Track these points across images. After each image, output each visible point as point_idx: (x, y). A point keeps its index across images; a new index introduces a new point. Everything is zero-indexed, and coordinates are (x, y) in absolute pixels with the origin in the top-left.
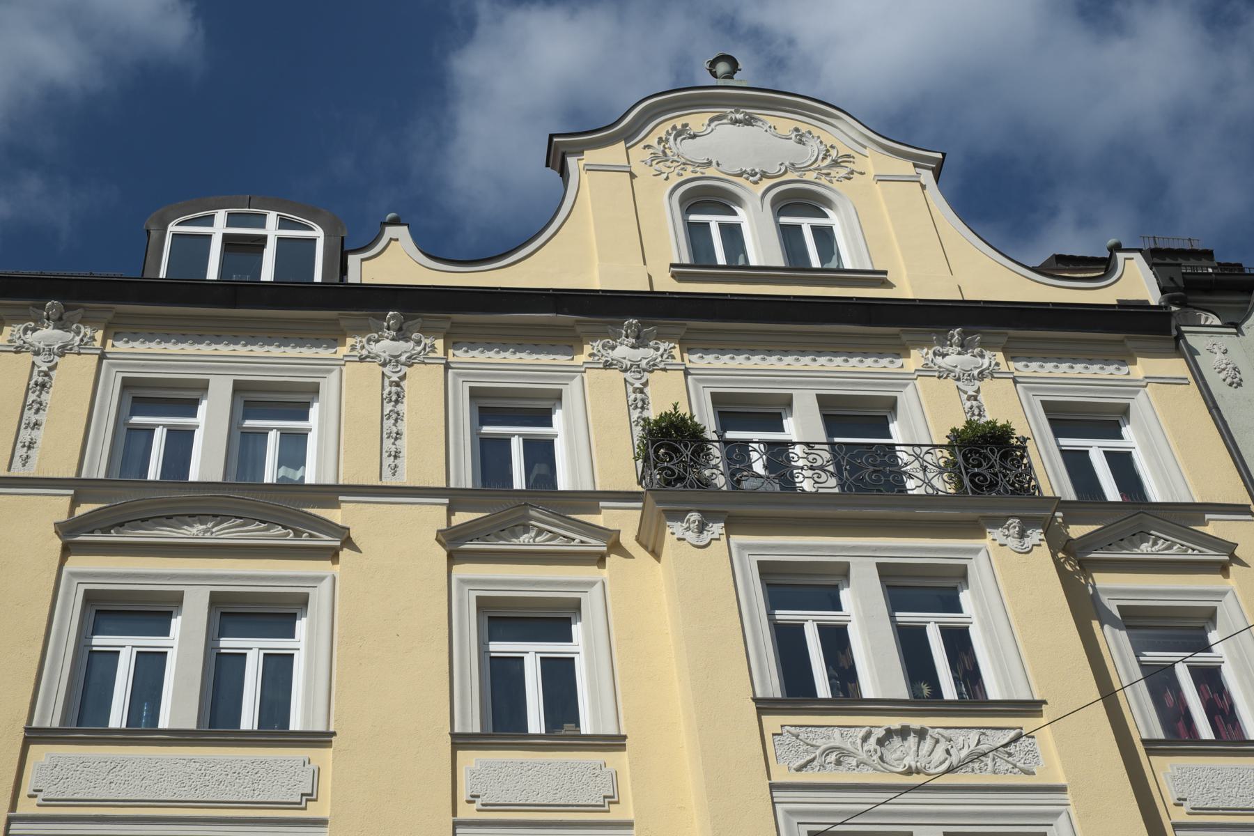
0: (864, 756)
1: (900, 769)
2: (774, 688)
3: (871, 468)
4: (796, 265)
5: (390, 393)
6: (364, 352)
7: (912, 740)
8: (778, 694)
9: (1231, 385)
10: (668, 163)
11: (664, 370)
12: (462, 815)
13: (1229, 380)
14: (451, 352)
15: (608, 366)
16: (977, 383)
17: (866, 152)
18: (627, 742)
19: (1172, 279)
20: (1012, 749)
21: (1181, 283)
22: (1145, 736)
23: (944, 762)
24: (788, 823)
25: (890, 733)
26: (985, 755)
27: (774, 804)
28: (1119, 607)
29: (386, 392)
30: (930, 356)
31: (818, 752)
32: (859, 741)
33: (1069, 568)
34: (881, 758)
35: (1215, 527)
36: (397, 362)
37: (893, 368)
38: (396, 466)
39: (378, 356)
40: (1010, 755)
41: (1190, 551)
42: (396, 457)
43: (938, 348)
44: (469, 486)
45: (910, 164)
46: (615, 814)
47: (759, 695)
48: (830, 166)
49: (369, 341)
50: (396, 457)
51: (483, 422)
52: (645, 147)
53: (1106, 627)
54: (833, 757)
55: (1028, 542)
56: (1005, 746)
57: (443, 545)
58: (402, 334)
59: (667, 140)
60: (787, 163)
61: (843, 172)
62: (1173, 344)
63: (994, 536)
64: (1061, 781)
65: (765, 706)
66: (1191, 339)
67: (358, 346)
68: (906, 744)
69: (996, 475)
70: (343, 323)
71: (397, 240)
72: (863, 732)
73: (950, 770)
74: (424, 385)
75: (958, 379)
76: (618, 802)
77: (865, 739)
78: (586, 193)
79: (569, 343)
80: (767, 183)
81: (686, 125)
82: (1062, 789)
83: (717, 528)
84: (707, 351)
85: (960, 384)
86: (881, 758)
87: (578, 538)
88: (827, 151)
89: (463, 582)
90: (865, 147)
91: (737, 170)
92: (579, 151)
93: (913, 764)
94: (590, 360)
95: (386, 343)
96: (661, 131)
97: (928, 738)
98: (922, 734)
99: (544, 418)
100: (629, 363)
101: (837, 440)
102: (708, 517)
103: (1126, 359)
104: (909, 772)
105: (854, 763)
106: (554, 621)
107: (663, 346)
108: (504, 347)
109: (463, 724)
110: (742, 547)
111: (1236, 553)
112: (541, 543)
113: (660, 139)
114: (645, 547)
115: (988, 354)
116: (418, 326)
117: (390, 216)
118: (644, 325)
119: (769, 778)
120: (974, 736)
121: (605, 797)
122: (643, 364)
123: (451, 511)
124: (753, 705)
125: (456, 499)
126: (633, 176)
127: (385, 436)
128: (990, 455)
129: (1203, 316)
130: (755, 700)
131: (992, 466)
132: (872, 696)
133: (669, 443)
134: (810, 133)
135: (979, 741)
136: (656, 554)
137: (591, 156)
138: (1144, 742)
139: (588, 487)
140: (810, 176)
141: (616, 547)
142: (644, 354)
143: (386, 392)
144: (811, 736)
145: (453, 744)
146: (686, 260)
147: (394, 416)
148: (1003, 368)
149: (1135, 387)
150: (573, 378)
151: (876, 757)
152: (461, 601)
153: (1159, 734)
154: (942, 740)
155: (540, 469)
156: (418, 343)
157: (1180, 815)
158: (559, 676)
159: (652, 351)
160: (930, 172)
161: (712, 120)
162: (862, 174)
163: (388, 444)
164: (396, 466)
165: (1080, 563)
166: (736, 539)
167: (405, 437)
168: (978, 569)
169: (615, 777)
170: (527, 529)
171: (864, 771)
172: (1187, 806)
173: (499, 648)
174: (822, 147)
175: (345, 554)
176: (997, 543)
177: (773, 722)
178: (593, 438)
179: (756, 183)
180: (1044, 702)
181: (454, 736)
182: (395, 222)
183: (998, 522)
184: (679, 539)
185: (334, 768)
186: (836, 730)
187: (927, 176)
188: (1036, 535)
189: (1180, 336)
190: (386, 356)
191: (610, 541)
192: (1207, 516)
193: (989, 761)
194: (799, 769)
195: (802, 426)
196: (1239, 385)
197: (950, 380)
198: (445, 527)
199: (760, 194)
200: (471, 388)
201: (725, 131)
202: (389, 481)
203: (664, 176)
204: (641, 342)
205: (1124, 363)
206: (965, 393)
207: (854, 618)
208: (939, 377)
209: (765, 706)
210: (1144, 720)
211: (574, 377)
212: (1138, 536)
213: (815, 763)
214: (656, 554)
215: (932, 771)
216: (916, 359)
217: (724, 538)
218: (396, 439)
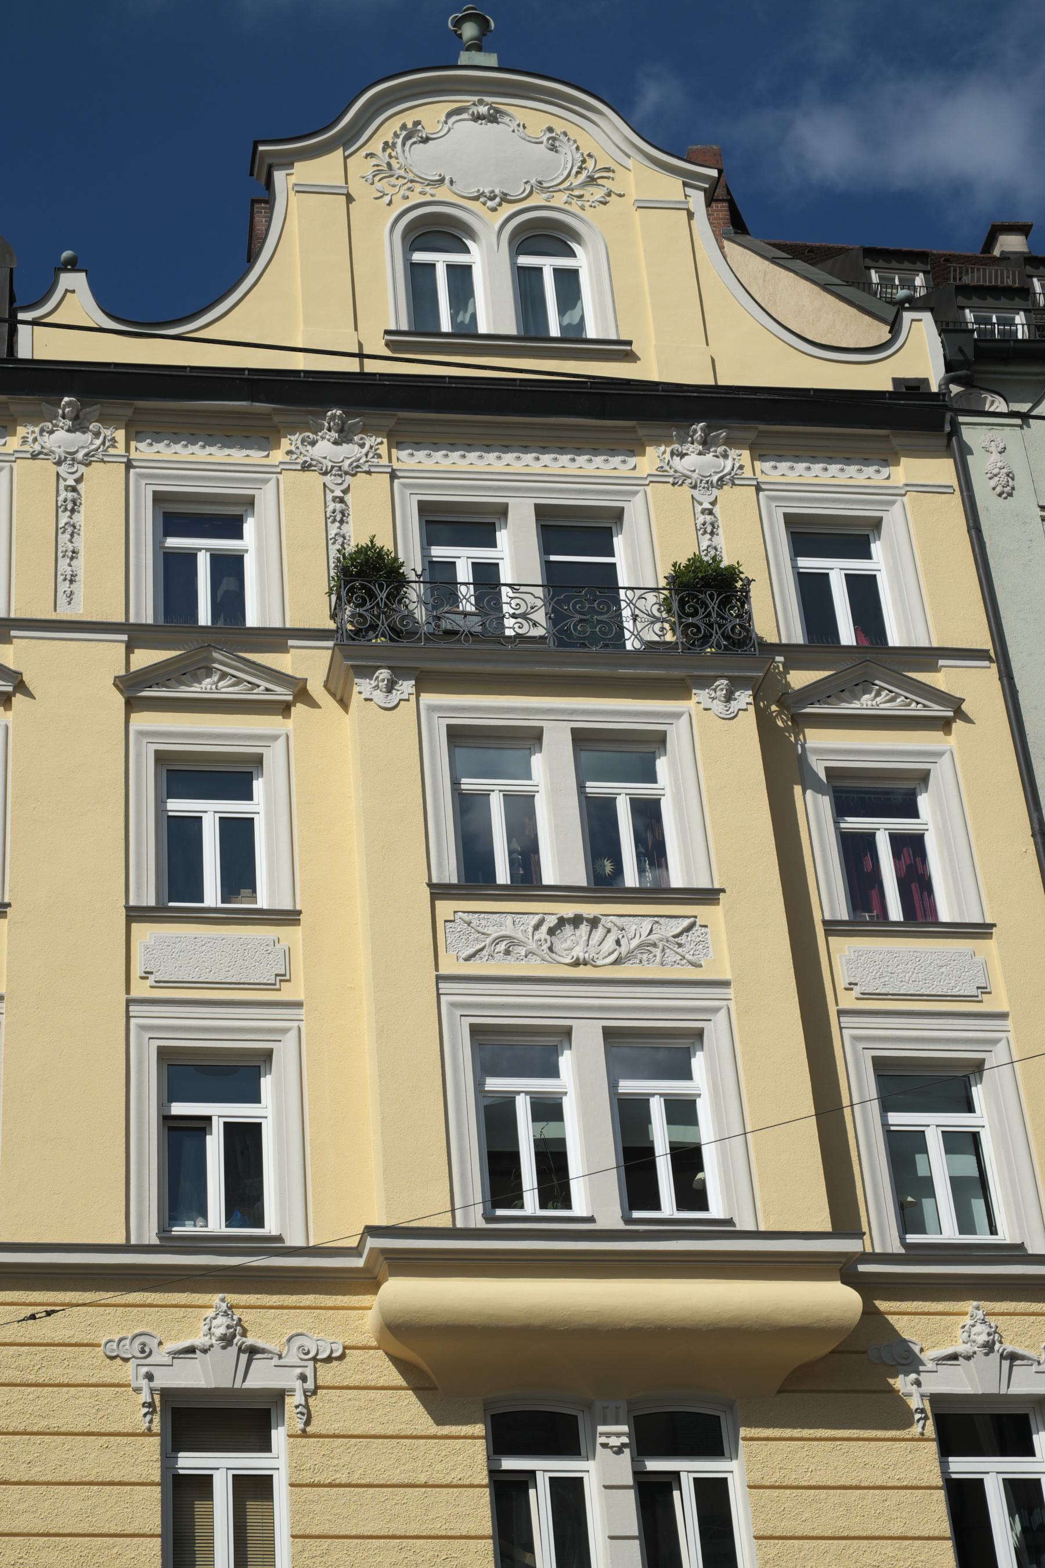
0: (533, 946)
1: (568, 960)
2: (449, 872)
3: (578, 617)
4: (531, 335)
5: (65, 501)
6: (37, 447)
7: (584, 928)
8: (454, 880)
9: (1000, 495)
10: (393, 180)
11: (369, 473)
12: (135, 994)
13: (999, 489)
14: (133, 444)
15: (306, 467)
16: (715, 492)
17: (629, 163)
18: (302, 917)
19: (961, 350)
20: (682, 940)
21: (971, 355)
22: (827, 917)
23: (613, 953)
24: (451, 1015)
25: (562, 922)
26: (655, 945)
27: (439, 995)
28: (827, 769)
29: (61, 499)
30: (667, 456)
31: (488, 941)
32: (530, 929)
33: (780, 723)
34: (551, 949)
35: (943, 678)
36: (73, 459)
37: (624, 470)
38: (72, 593)
39: (53, 452)
40: (680, 945)
41: (914, 704)
42: (71, 581)
43: (676, 446)
44: (150, 621)
45: (678, 182)
46: (286, 994)
47: (435, 881)
48: (584, 185)
49: (42, 431)
50: (71, 581)
51: (168, 533)
52: (367, 156)
53: (809, 792)
54: (502, 947)
55: (734, 706)
56: (675, 936)
57: (121, 691)
58: (78, 425)
59: (394, 144)
60: (533, 181)
61: (598, 193)
62: (945, 442)
63: (701, 696)
64: (727, 976)
65: (439, 891)
66: (969, 435)
67: (30, 440)
68: (578, 932)
69: (711, 626)
70: (13, 408)
71: (73, 292)
72: (534, 920)
73: (617, 962)
74: (102, 485)
75: (695, 487)
76: (289, 981)
77: (537, 927)
78: (294, 224)
79: (265, 436)
80: (508, 210)
81: (417, 123)
82: (726, 984)
83: (407, 687)
84: (418, 445)
85: (695, 493)
86: (551, 949)
87: (264, 684)
88: (584, 161)
89: (141, 734)
90: (629, 156)
91: (473, 191)
92: (288, 161)
93: (581, 956)
94: (287, 459)
95: (61, 435)
96: (387, 134)
97: (600, 926)
98: (594, 922)
99: (233, 527)
100: (330, 464)
101: (553, 558)
102: (399, 673)
103: (889, 459)
104: (576, 963)
105: (523, 953)
106: (233, 777)
107: (370, 441)
108: (192, 439)
109: (138, 896)
110: (432, 709)
111: (964, 707)
112: (226, 690)
113: (386, 143)
114: (333, 695)
115: (733, 453)
116: (97, 413)
117: (67, 254)
118: (349, 415)
119: (437, 969)
120: (647, 924)
121: (277, 975)
122: (346, 465)
123: (130, 649)
124: (426, 892)
125: (136, 636)
126: (350, 199)
127: (60, 555)
128: (708, 600)
129: (990, 399)
130: (430, 885)
131: (709, 615)
132: (552, 883)
133: (366, 577)
134: (565, 134)
135: (651, 931)
136: (344, 703)
137: (304, 171)
138: (825, 923)
139: (277, 624)
140: (559, 200)
141: (302, 694)
142: (350, 451)
143: (61, 499)
144: (484, 923)
145: (127, 916)
146: (404, 326)
147: (70, 530)
148: (748, 473)
149: (891, 495)
150: (266, 481)
151: (545, 947)
152: (138, 756)
153: (843, 913)
154: (614, 930)
155: (228, 584)
156: (97, 435)
157: (848, 1001)
158: (238, 836)
159: (356, 447)
160: (702, 194)
161: (449, 115)
162: (620, 196)
163: (63, 563)
164: (72, 593)
165: (794, 718)
166: (428, 699)
167: (82, 555)
168: (678, 735)
169: (288, 953)
170: (209, 672)
171: (532, 962)
172: (857, 990)
173: (178, 806)
174: (578, 156)
175: (18, 700)
176: (702, 706)
177: (446, 908)
178: (284, 575)
179: (494, 210)
180: (723, 891)
181: (128, 908)
182: (72, 266)
183: (705, 683)
184: (366, 700)
185: (9, 942)
186: (509, 917)
187: (697, 200)
188: (744, 698)
189: (956, 429)
190: (60, 452)
191: (296, 690)
192: (941, 662)
193: (658, 952)
194: (468, 959)
195: (515, 553)
196: (1010, 495)
197: (686, 488)
198: (123, 673)
199: (497, 227)
200: (154, 492)
201: (465, 128)
202: (65, 613)
203: (387, 199)
204: (344, 436)
205: (886, 462)
206: (701, 504)
207: (542, 789)
208: (674, 484)
209: (439, 891)
210: (829, 894)
211: (267, 481)
212: (860, 687)
213: (484, 952)
214: (344, 703)
215: (599, 963)
216: (651, 459)
217: (413, 698)
218: (72, 558)
